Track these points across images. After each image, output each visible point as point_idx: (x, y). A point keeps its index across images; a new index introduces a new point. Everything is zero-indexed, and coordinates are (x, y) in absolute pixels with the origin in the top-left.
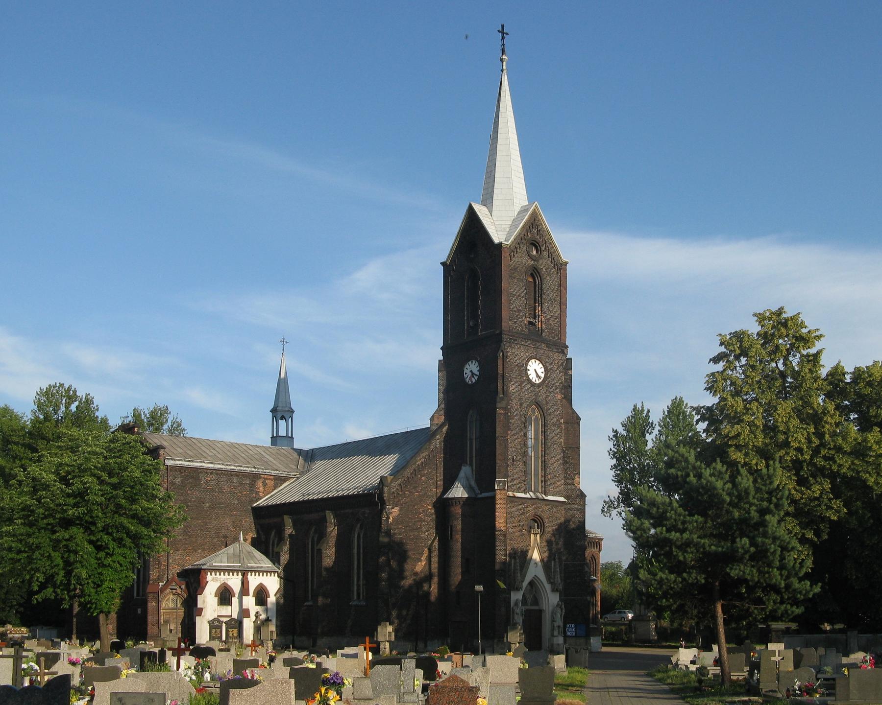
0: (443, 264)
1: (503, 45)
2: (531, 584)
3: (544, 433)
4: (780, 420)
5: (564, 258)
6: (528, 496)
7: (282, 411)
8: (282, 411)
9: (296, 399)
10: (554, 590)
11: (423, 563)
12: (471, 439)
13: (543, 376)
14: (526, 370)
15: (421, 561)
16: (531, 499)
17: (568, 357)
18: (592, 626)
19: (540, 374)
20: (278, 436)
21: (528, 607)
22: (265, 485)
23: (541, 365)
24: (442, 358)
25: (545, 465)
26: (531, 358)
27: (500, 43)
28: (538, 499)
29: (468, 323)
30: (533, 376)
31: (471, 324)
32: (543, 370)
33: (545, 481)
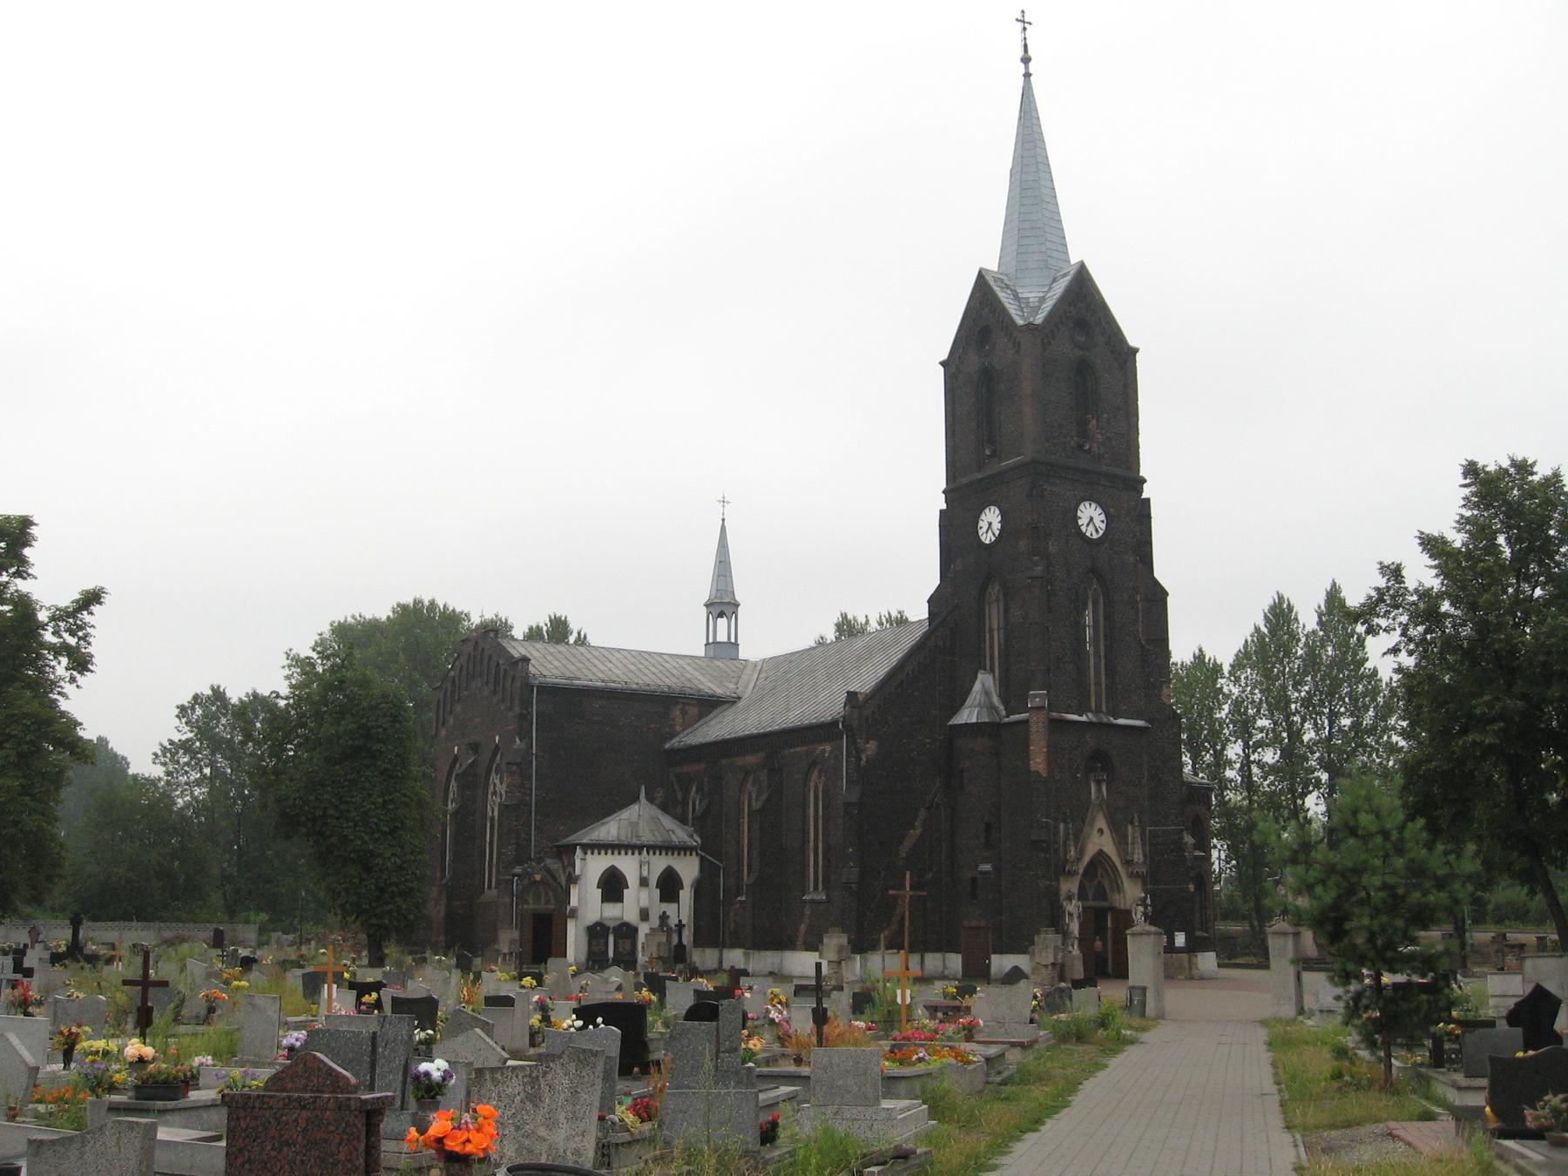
0: (942, 364)
1: (1027, 75)
2: (1093, 864)
3: (1107, 617)
4: (388, 854)
5: (1132, 342)
6: (1084, 718)
7: (722, 606)
8: (722, 606)
9: (742, 591)
10: (1131, 876)
11: (918, 832)
12: (991, 631)
13: (1103, 526)
14: (1076, 518)
15: (914, 828)
16: (1090, 723)
17: (1144, 496)
18: (1199, 933)
19: (1098, 524)
20: (715, 643)
21: (1091, 903)
22: (684, 713)
23: (1099, 510)
24: (944, 506)
25: (1111, 671)
26: (1084, 499)
27: (1020, 36)
28: (1101, 725)
29: (1105, 945)
30: (1090, 532)
31: (1098, 944)
32: (1103, 517)
33: (1111, 694)
